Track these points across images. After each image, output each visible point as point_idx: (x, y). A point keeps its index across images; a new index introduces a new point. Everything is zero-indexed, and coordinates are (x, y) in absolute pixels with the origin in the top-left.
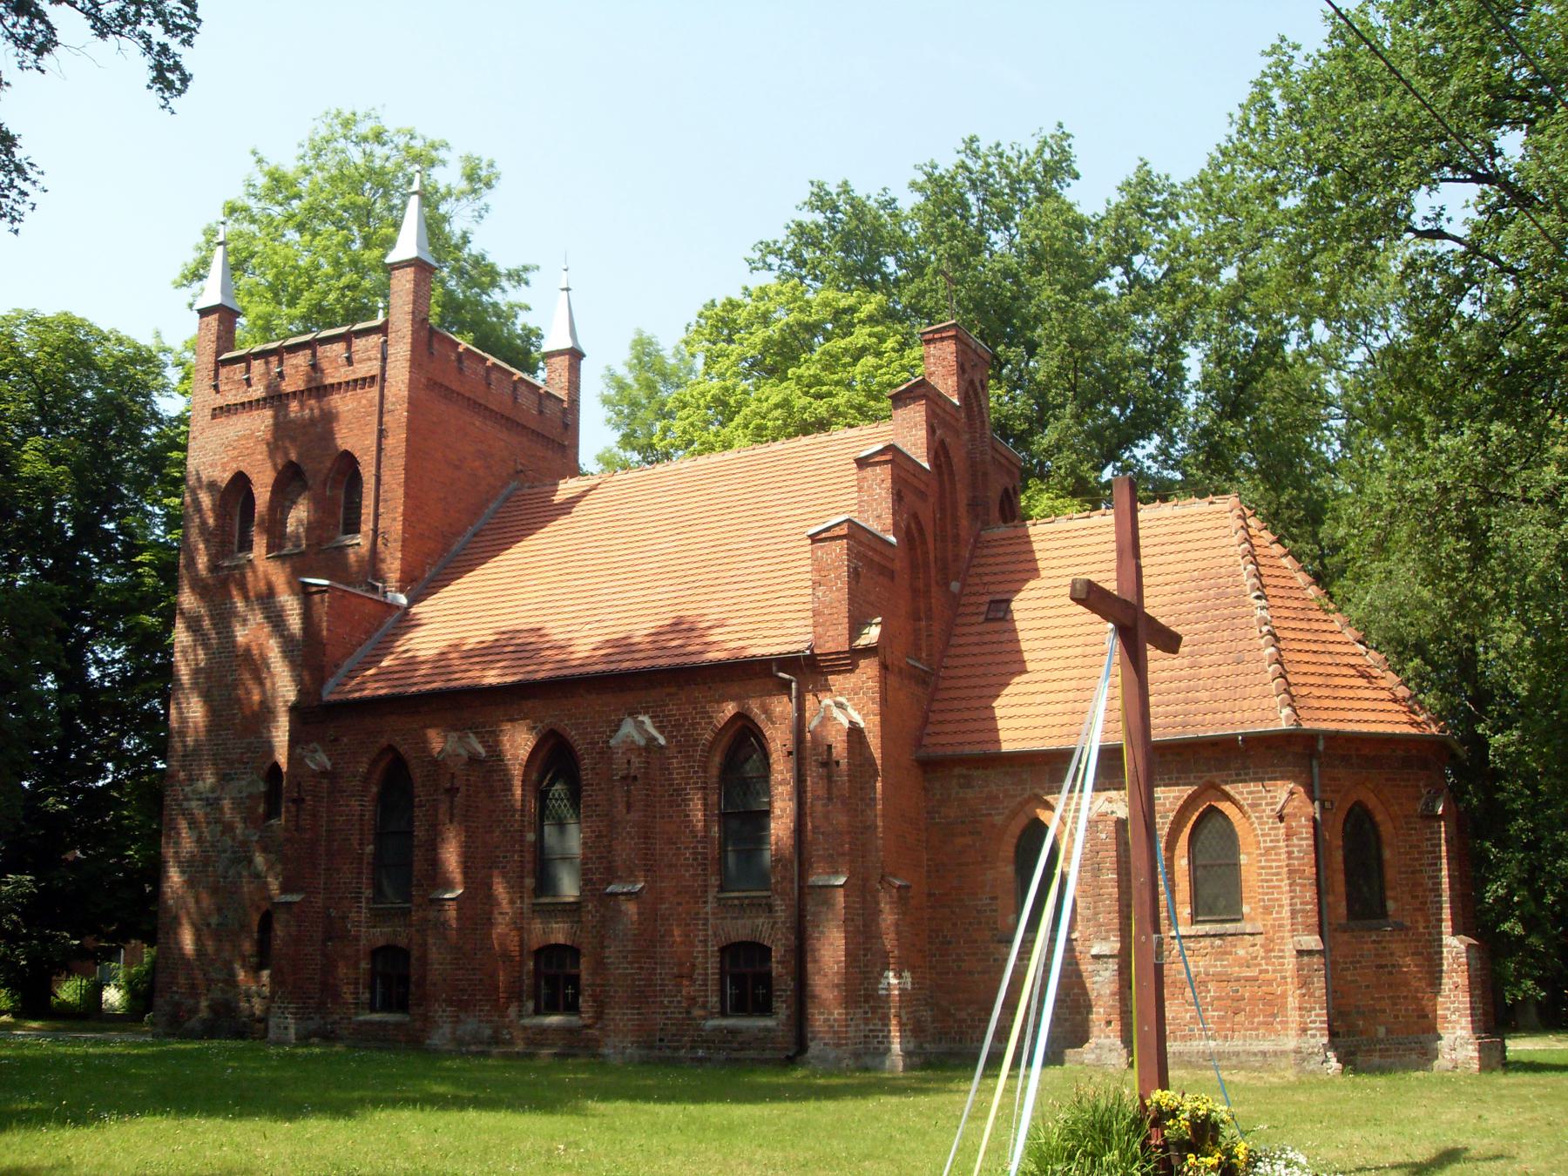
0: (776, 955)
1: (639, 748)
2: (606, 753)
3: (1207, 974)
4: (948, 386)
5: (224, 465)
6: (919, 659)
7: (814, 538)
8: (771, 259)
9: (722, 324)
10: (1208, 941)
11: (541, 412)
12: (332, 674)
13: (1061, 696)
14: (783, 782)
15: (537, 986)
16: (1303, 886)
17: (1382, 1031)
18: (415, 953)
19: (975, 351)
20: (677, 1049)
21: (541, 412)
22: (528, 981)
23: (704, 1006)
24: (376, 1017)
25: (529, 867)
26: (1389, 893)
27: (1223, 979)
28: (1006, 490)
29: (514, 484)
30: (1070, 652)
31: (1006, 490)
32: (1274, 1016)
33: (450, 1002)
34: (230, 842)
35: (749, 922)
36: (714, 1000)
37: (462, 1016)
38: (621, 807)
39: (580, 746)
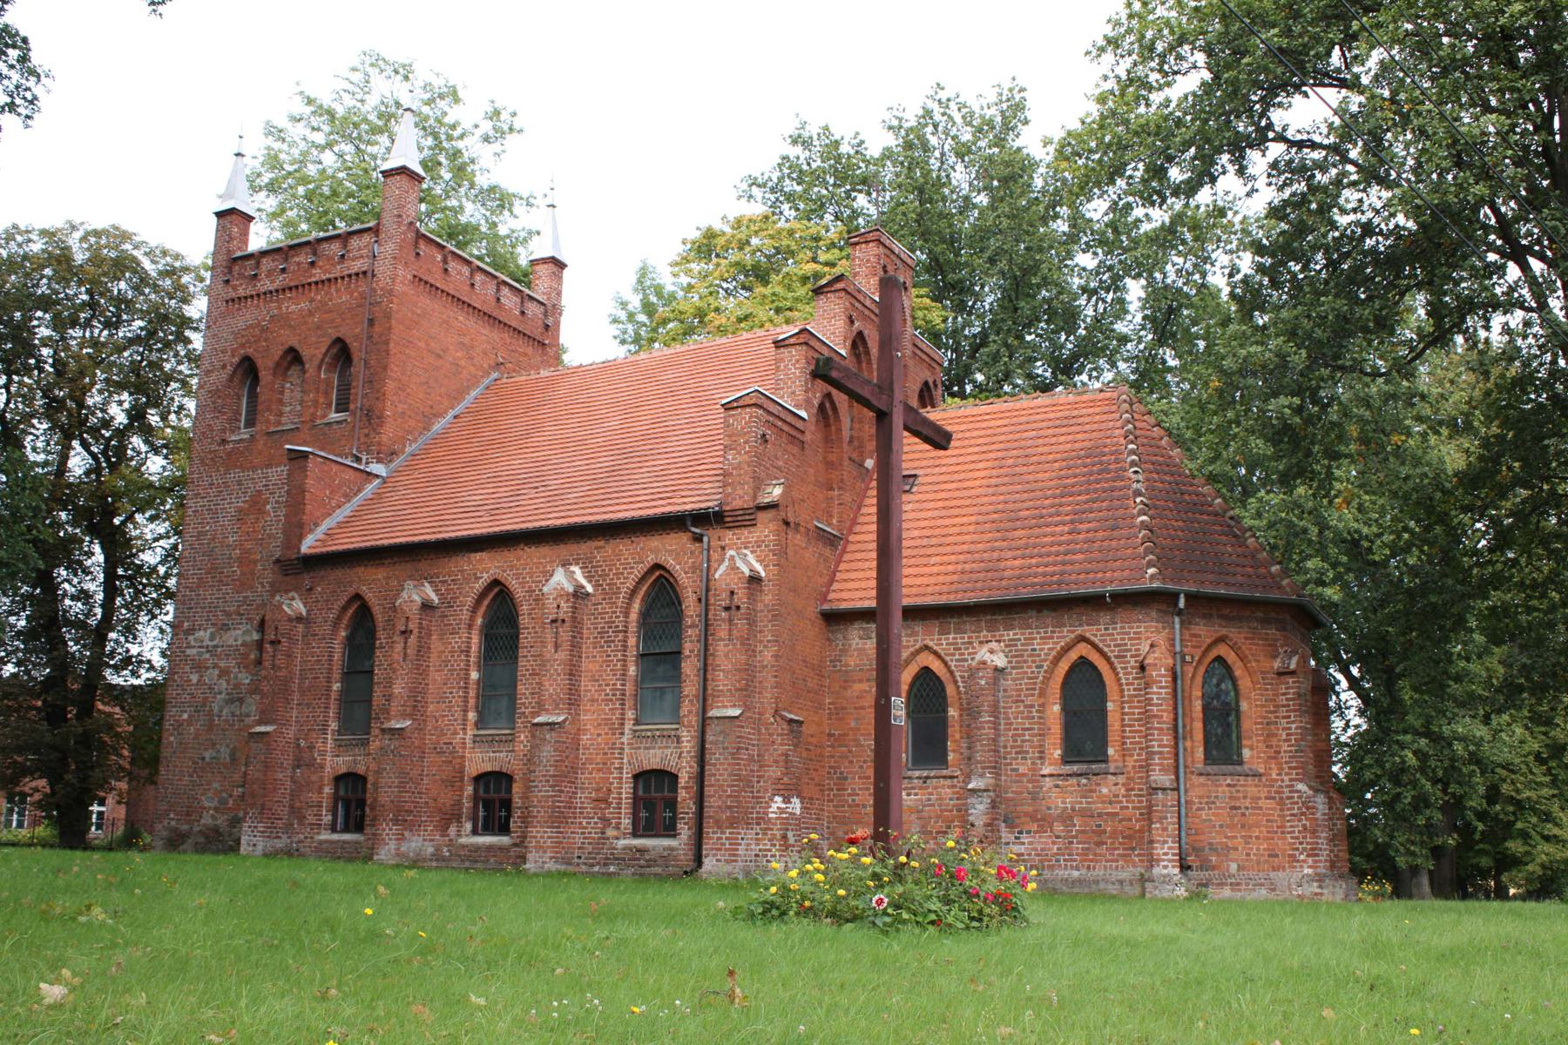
0: (682, 781)
1: (568, 594)
2: (539, 599)
3: (1073, 809)
4: (869, 287)
5: (233, 351)
6: (829, 525)
7: (727, 407)
8: (755, 191)
9: (706, 246)
10: (1074, 781)
11: (523, 313)
12: (311, 531)
13: (953, 558)
14: (693, 626)
15: (476, 807)
16: (1161, 729)
17: (1233, 867)
18: (371, 779)
19: (898, 257)
20: (592, 865)
21: (523, 313)
22: (467, 804)
23: (617, 828)
24: (335, 837)
25: (472, 702)
26: (1244, 742)
27: (1086, 814)
28: (926, 383)
29: (495, 375)
30: (965, 520)
31: (926, 383)
32: (1133, 849)
33: (396, 821)
34: (225, 685)
35: (659, 752)
36: (626, 822)
37: (406, 833)
38: (550, 647)
39: (519, 593)
